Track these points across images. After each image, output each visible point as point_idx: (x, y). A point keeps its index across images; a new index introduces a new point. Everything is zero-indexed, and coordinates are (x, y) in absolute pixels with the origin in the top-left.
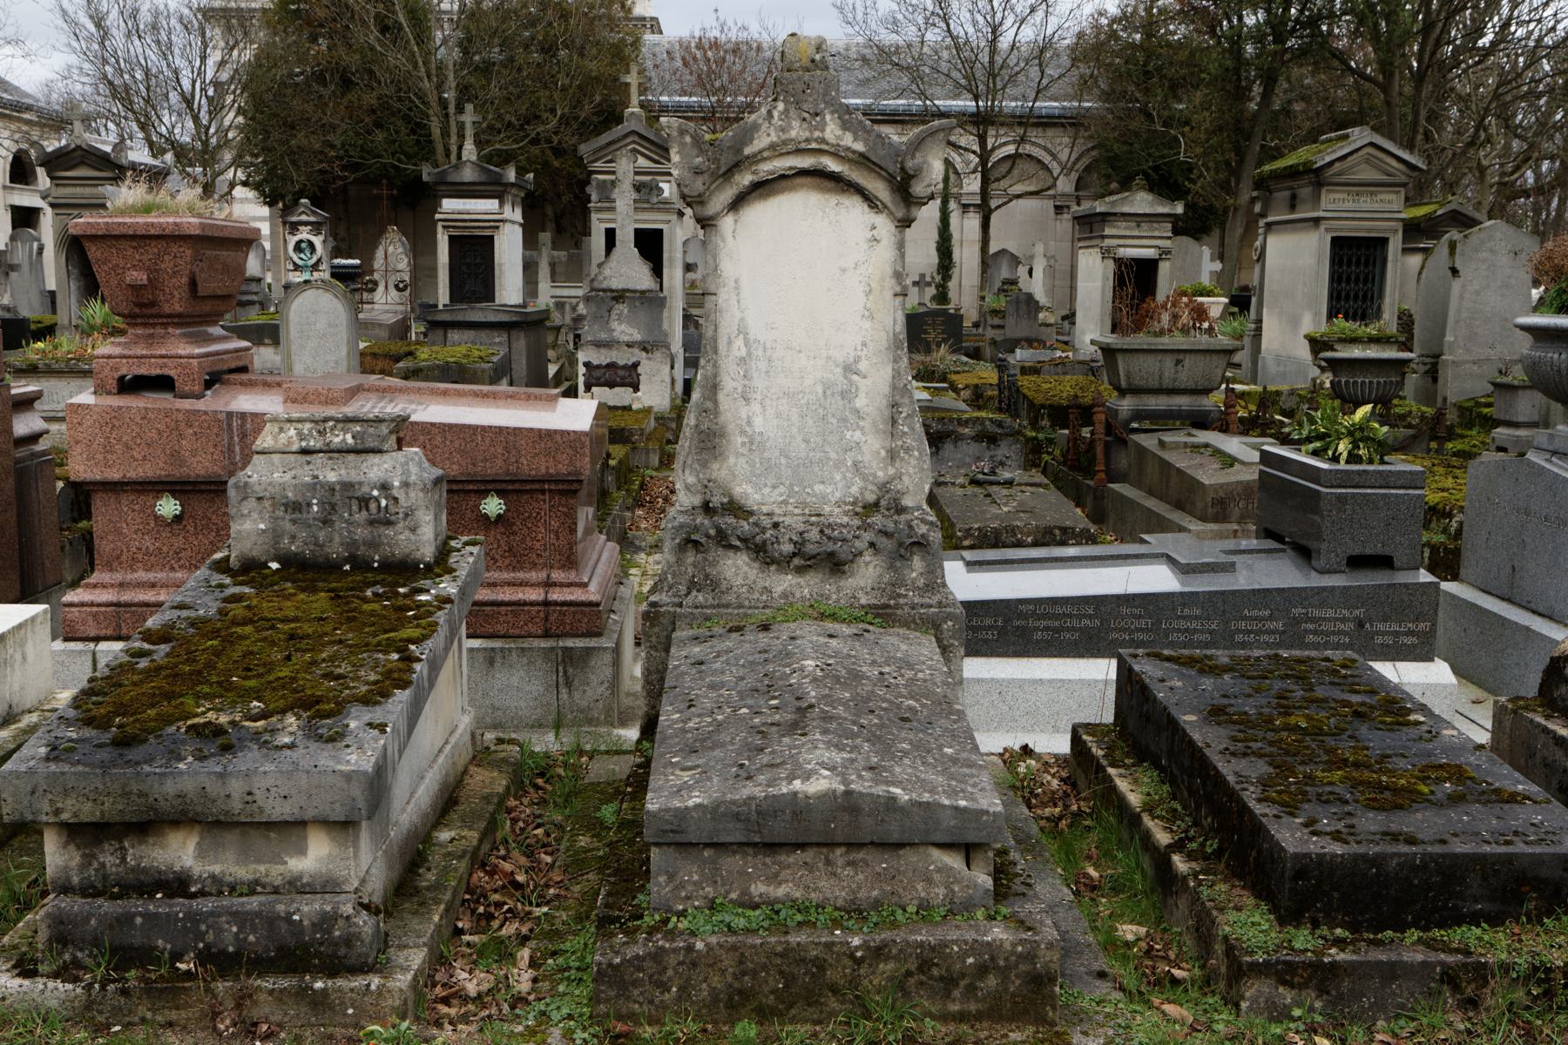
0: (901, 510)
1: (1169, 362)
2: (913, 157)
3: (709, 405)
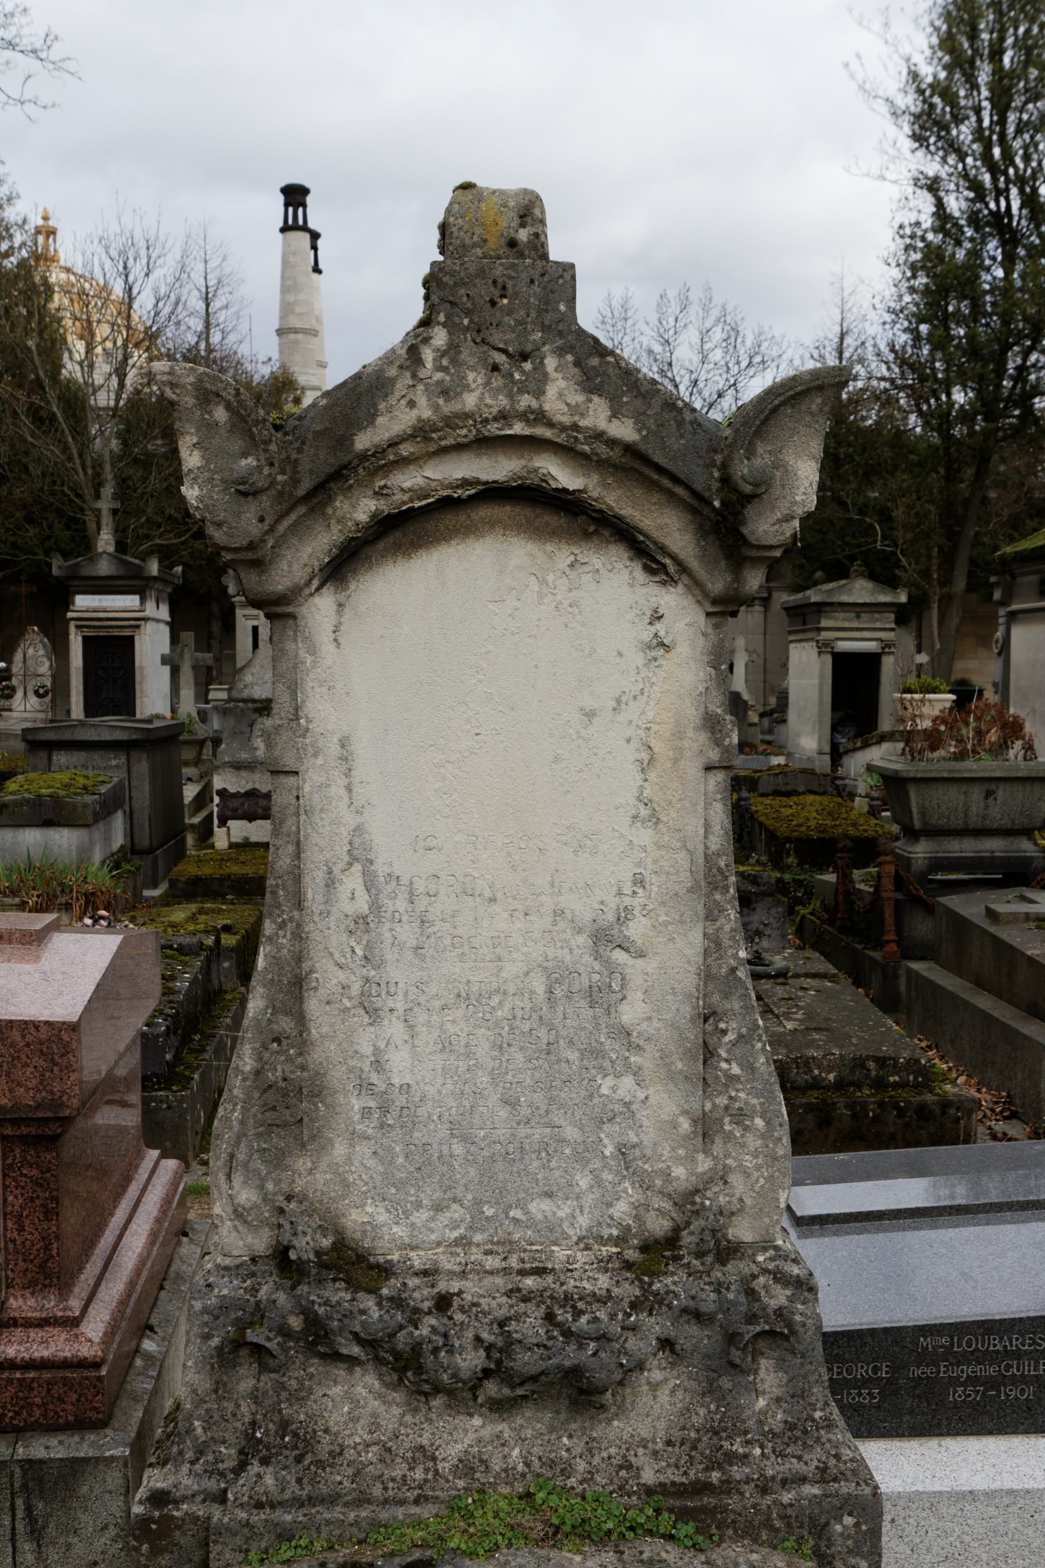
0: (728, 1252)
1: (977, 794)
2: (750, 454)
3: (286, 1024)
